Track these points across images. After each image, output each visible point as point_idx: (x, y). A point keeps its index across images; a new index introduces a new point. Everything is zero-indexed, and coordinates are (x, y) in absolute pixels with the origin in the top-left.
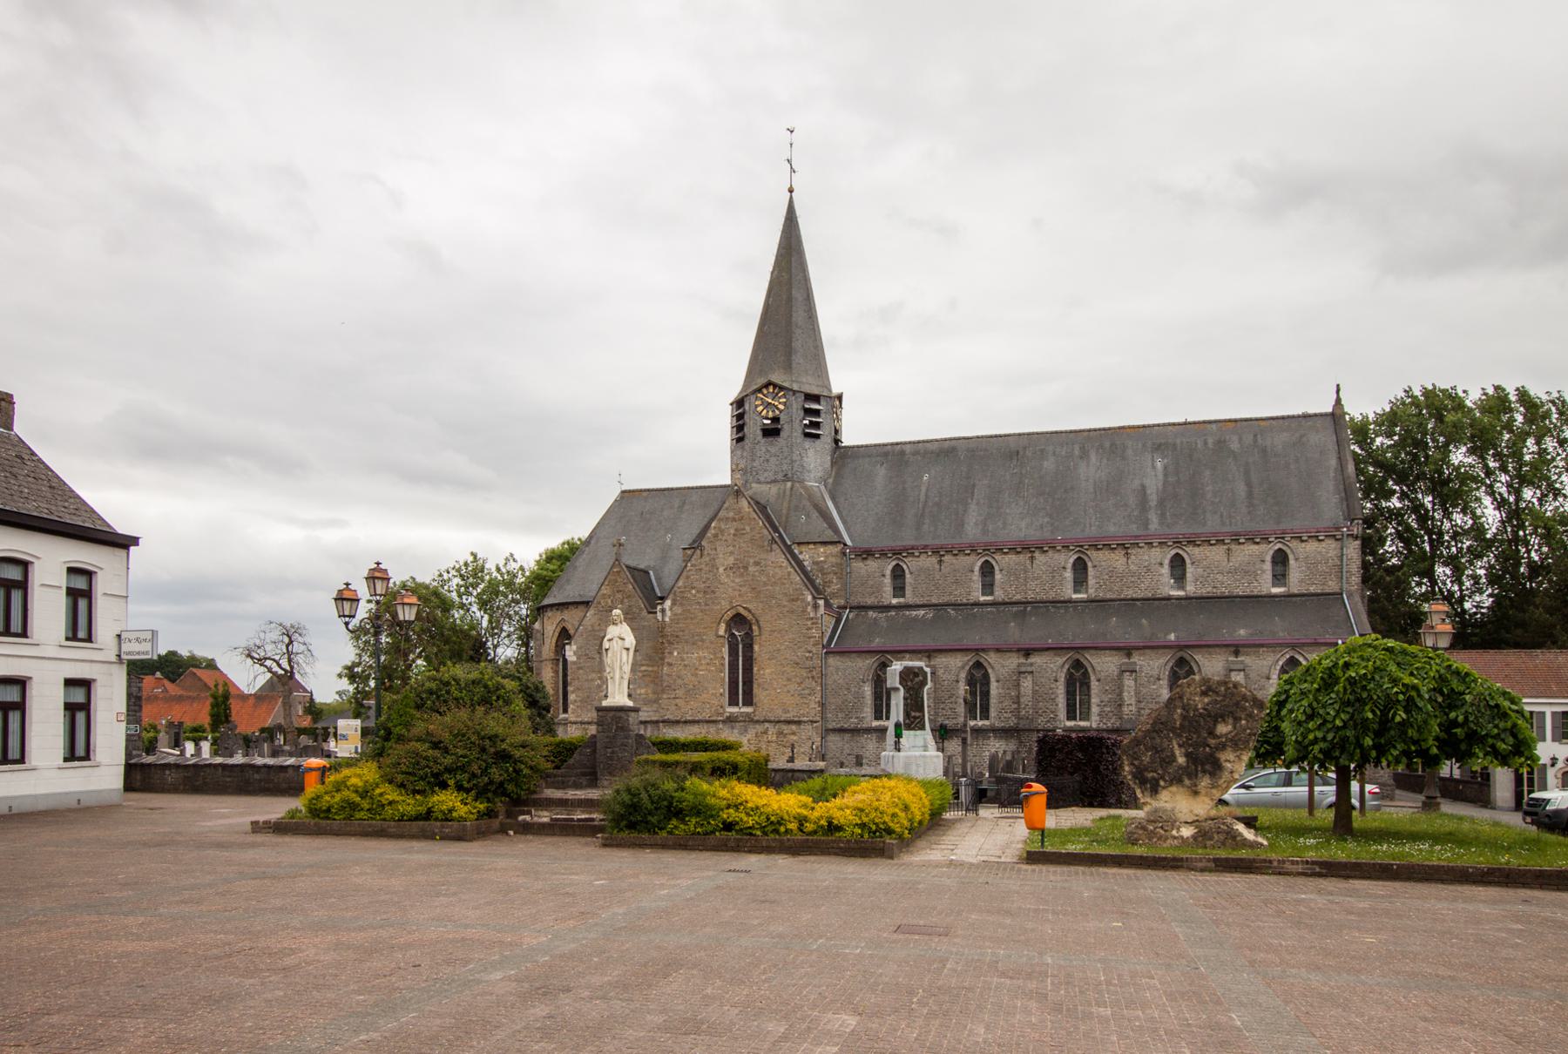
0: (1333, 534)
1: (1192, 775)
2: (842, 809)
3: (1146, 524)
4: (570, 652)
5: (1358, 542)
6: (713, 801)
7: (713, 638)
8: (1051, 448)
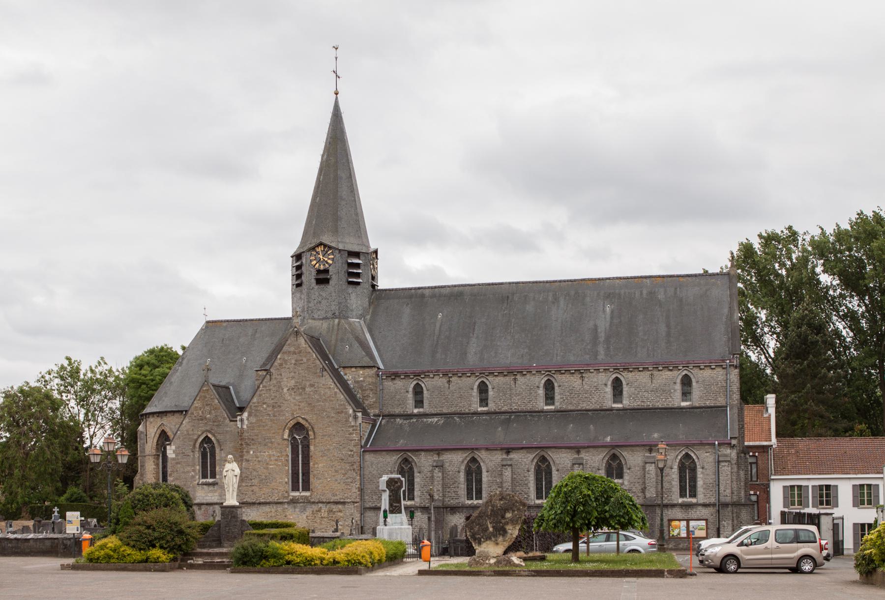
0: (720, 364)
1: (495, 536)
2: (339, 554)
3: (596, 354)
4: (170, 451)
5: (737, 370)
6: (281, 551)
7: (280, 441)
8: (531, 295)
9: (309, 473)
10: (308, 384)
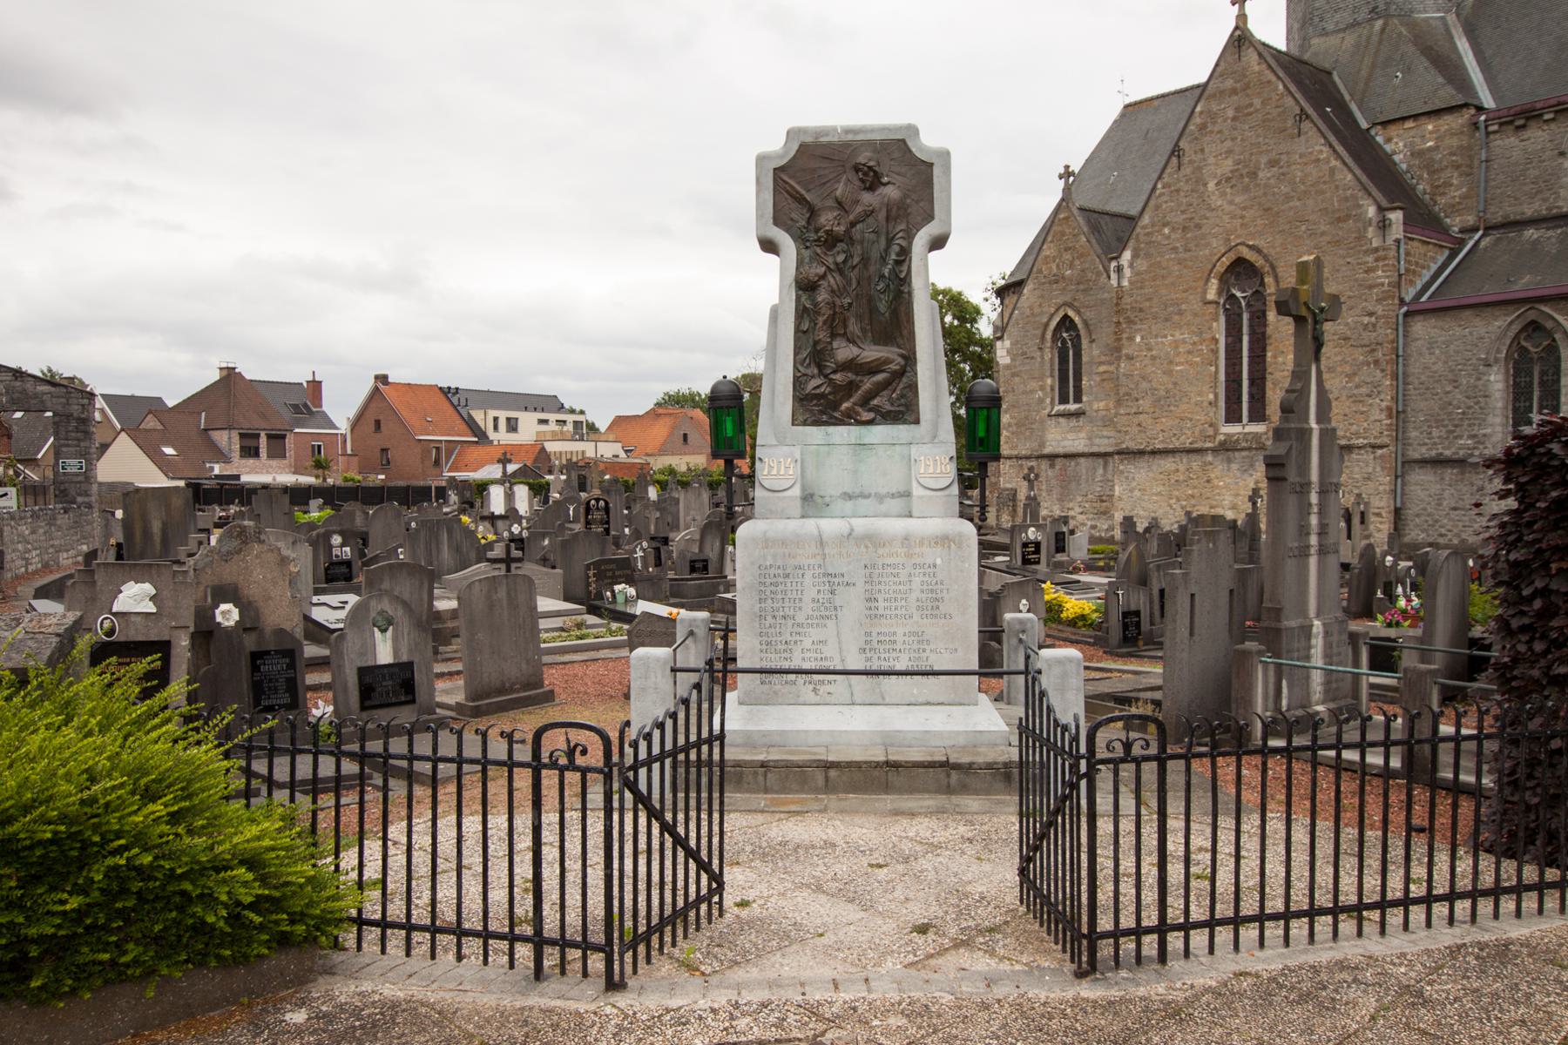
7: (1197, 306)
9: (1264, 379)
10: (1264, 160)
